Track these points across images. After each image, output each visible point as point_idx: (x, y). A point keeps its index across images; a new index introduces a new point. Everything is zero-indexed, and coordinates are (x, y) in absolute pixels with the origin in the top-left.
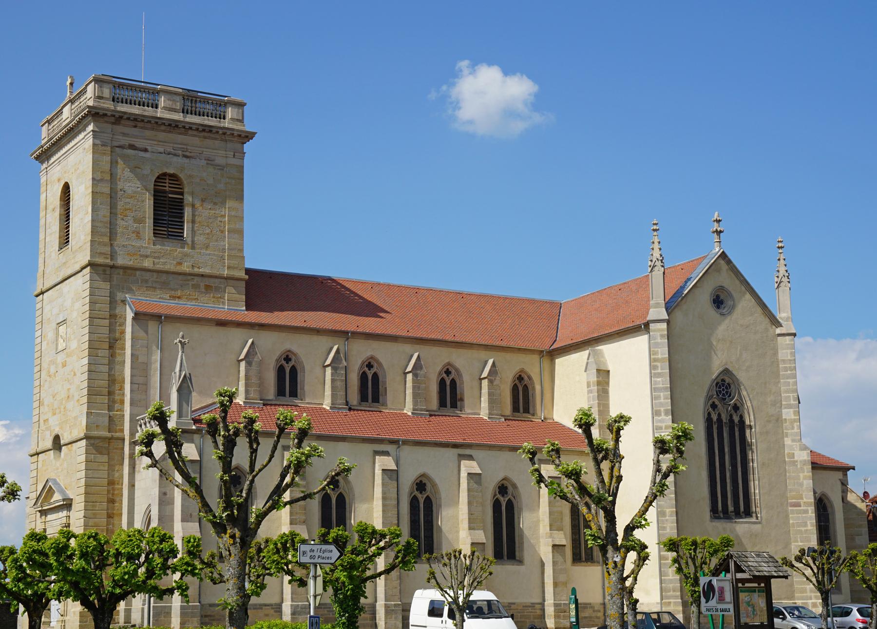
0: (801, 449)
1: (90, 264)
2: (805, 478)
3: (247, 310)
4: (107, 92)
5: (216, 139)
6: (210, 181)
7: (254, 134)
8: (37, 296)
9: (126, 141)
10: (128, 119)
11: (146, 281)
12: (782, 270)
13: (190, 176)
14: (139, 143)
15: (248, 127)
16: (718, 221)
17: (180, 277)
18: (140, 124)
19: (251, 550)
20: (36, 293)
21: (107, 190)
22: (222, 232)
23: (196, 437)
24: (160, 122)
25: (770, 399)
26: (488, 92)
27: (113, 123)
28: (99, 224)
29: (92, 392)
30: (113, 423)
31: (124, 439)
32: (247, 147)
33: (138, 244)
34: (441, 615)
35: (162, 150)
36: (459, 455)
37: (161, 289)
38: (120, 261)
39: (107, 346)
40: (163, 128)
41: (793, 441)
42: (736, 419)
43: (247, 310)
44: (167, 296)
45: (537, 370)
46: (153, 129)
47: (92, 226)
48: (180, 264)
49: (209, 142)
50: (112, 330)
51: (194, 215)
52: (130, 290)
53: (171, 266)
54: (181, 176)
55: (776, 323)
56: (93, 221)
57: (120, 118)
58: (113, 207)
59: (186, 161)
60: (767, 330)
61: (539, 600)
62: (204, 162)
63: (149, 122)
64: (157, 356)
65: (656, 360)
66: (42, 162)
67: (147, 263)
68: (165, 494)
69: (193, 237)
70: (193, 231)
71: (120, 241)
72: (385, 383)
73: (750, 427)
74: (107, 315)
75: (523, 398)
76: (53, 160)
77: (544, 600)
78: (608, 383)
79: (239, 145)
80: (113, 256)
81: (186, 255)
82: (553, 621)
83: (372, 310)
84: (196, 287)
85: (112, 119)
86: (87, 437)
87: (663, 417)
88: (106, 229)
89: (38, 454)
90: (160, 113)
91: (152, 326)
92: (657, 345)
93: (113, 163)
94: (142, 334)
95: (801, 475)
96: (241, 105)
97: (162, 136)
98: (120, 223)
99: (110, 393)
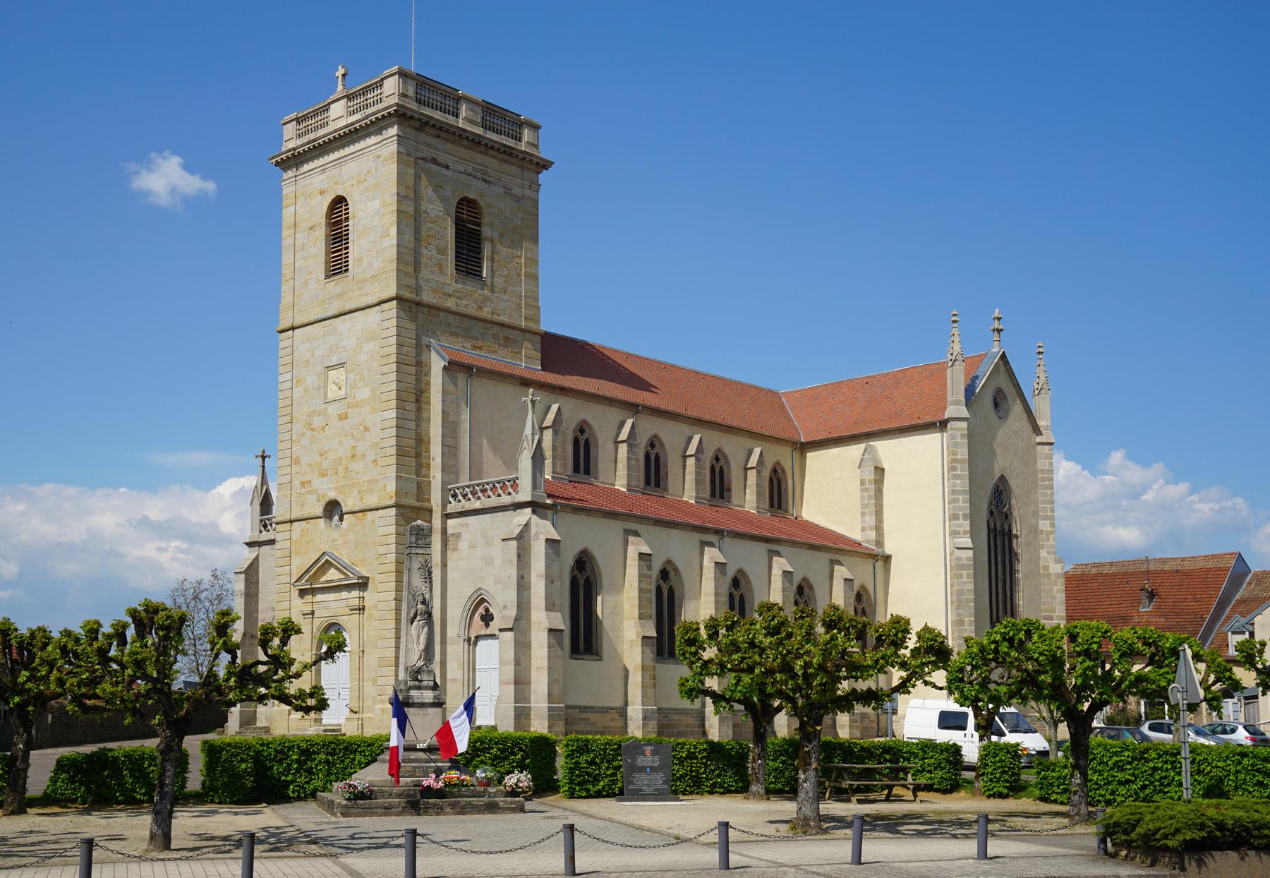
0: (1056, 562)
1: (398, 298)
2: (1058, 591)
3: (543, 369)
4: (411, 91)
5: (513, 164)
6: (508, 214)
7: (551, 163)
8: (281, 332)
9: (427, 152)
10: (434, 126)
11: (450, 325)
12: (1043, 376)
13: (489, 205)
14: (442, 158)
15: (544, 153)
16: (999, 319)
17: (481, 324)
18: (443, 135)
19: (902, 651)
20: (281, 327)
21: (411, 210)
22: (519, 275)
23: (549, 513)
24: (465, 135)
25: (1031, 509)
26: (165, 178)
27: (417, 129)
28: (404, 251)
29: (401, 453)
30: (422, 490)
31: (431, 511)
32: (544, 177)
33: (441, 279)
34: (963, 728)
35: (462, 169)
36: (770, 551)
37: (463, 336)
38: (427, 297)
39: (413, 398)
40: (465, 142)
41: (1049, 553)
42: (1007, 528)
43: (543, 369)
44: (469, 345)
45: (790, 463)
46: (454, 143)
47: (398, 252)
48: (480, 308)
49: (506, 167)
50: (418, 381)
51: (493, 252)
52: (434, 335)
53: (471, 310)
54: (481, 203)
55: (1037, 430)
56: (398, 245)
57: (428, 123)
58: (417, 231)
59: (486, 186)
60: (1030, 438)
61: (619, 703)
62: (501, 190)
63: (454, 133)
64: (466, 415)
65: (954, 461)
66: (285, 170)
67: (450, 304)
68: (522, 577)
69: (493, 277)
70: (492, 272)
71: (425, 273)
72: (666, 466)
73: (1017, 537)
74: (413, 361)
75: (778, 492)
76: (306, 167)
77: (626, 704)
78: (882, 482)
79: (534, 175)
80: (418, 290)
81: (487, 299)
82: (847, 730)
83: (644, 385)
84: (495, 337)
85: (417, 124)
86: (397, 506)
87: (961, 521)
88: (410, 258)
89: (291, 522)
90: (461, 124)
91: (461, 378)
92: (956, 445)
93: (417, 178)
94: (452, 387)
95: (1055, 588)
96: (535, 127)
97: (463, 152)
98: (424, 252)
99: (418, 455)
